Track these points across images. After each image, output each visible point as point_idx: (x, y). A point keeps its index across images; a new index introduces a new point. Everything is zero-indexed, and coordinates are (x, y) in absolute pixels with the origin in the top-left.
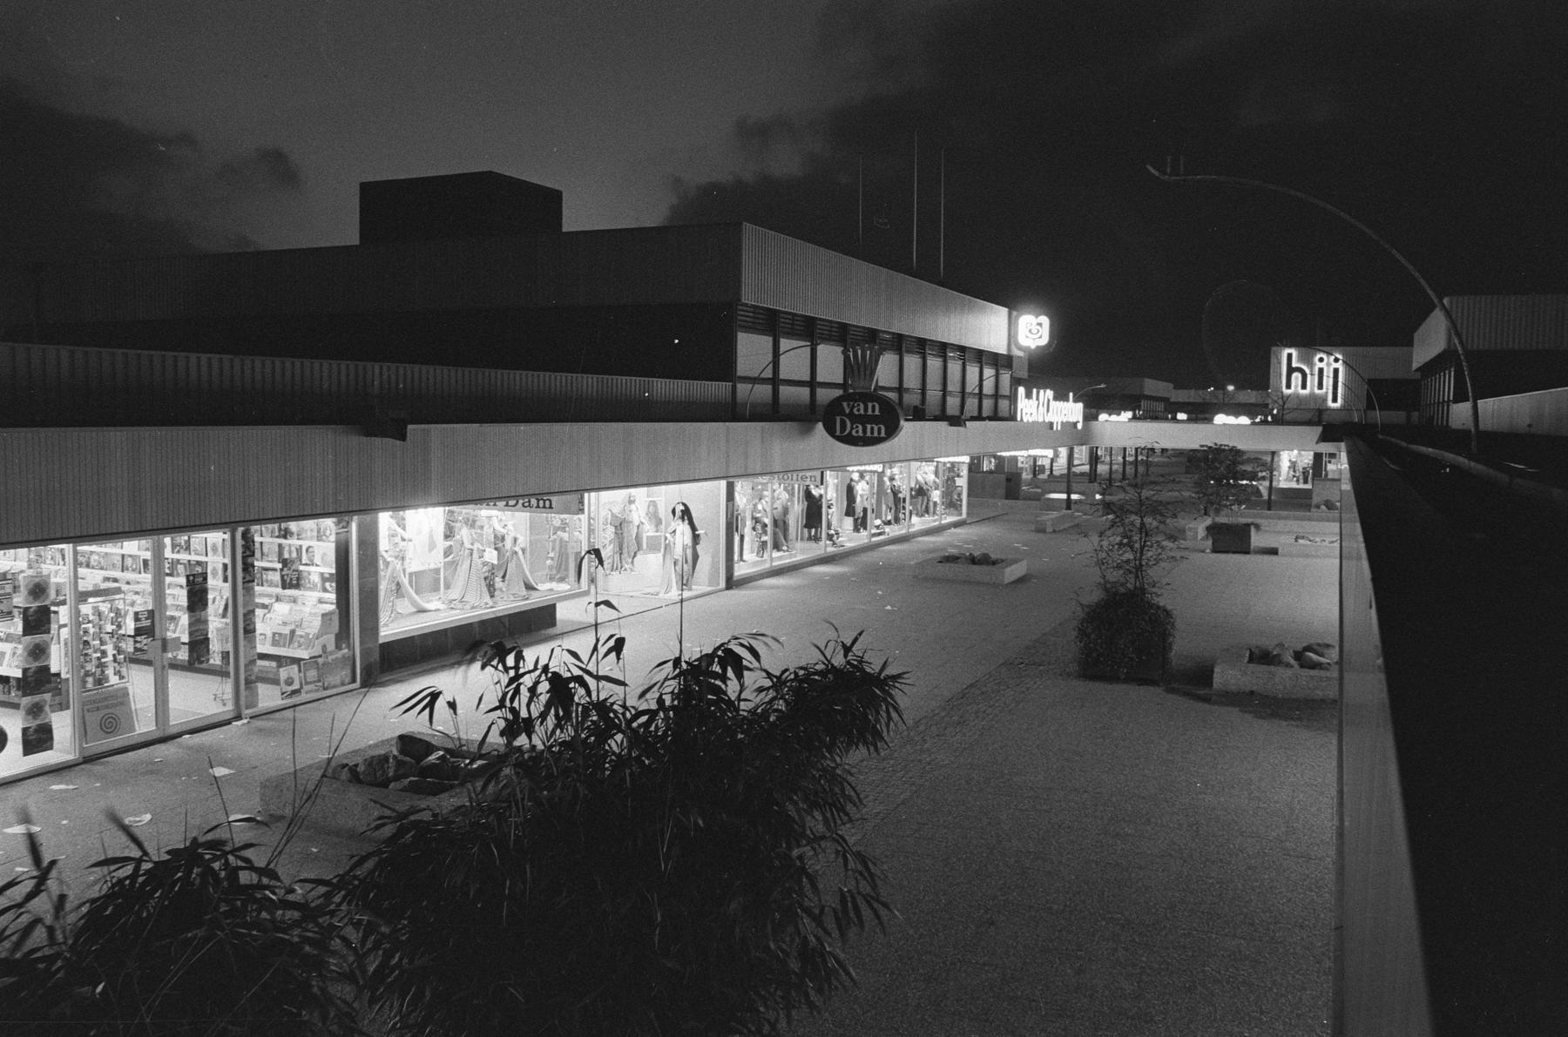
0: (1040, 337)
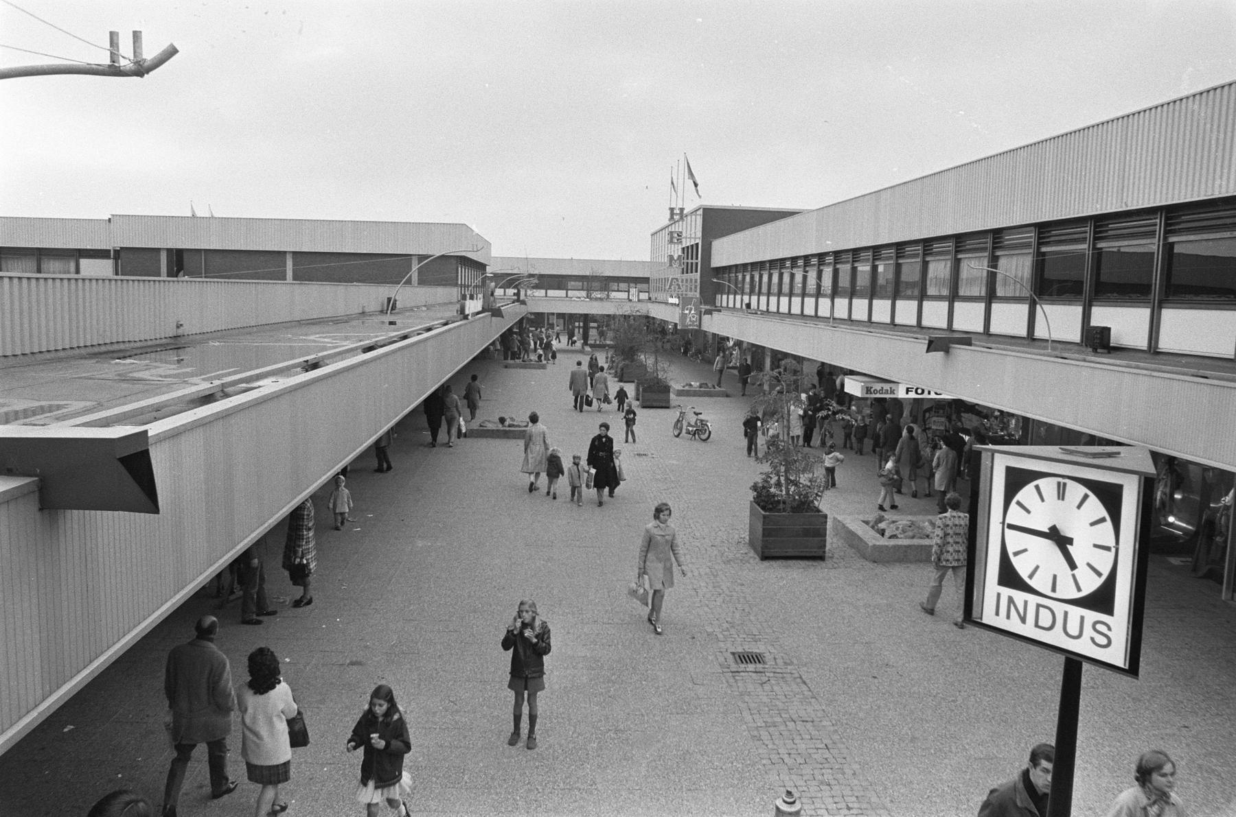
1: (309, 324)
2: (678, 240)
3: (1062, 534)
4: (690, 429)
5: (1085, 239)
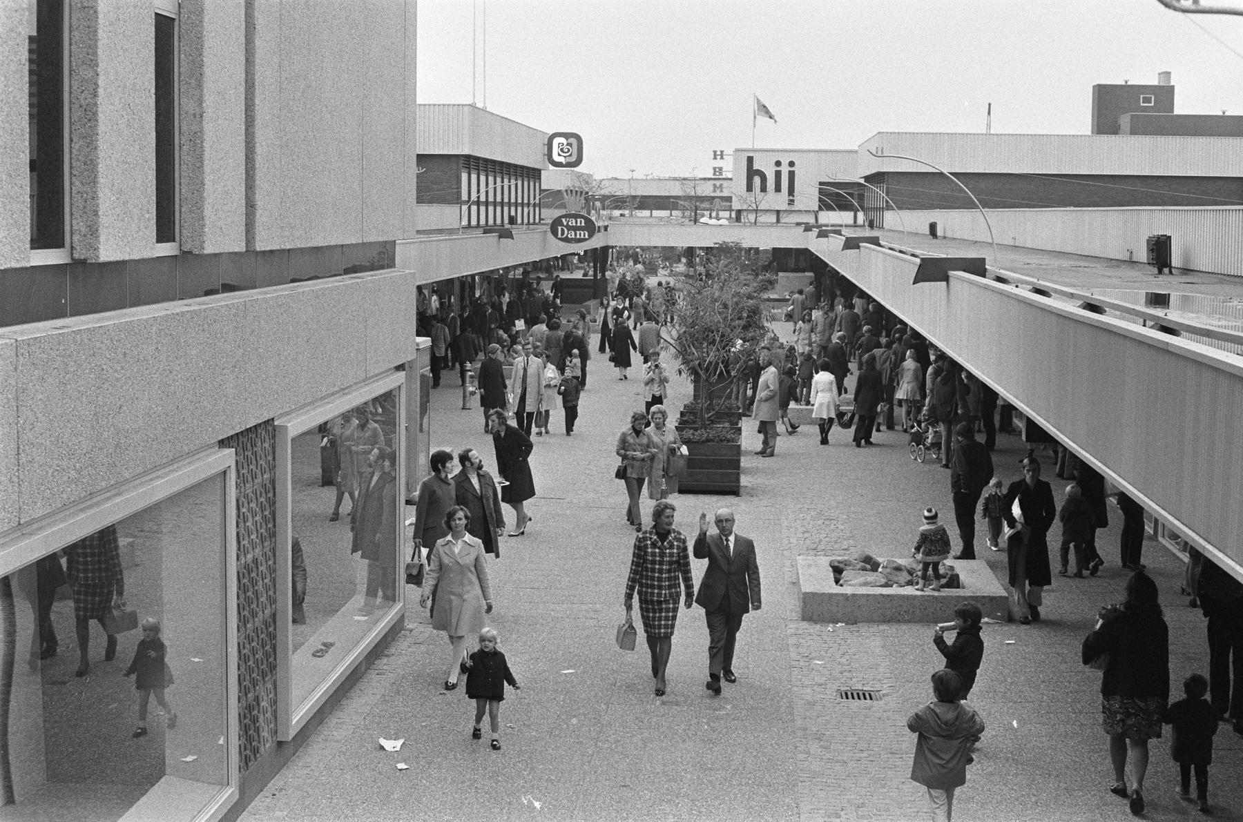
0: (571, 155)
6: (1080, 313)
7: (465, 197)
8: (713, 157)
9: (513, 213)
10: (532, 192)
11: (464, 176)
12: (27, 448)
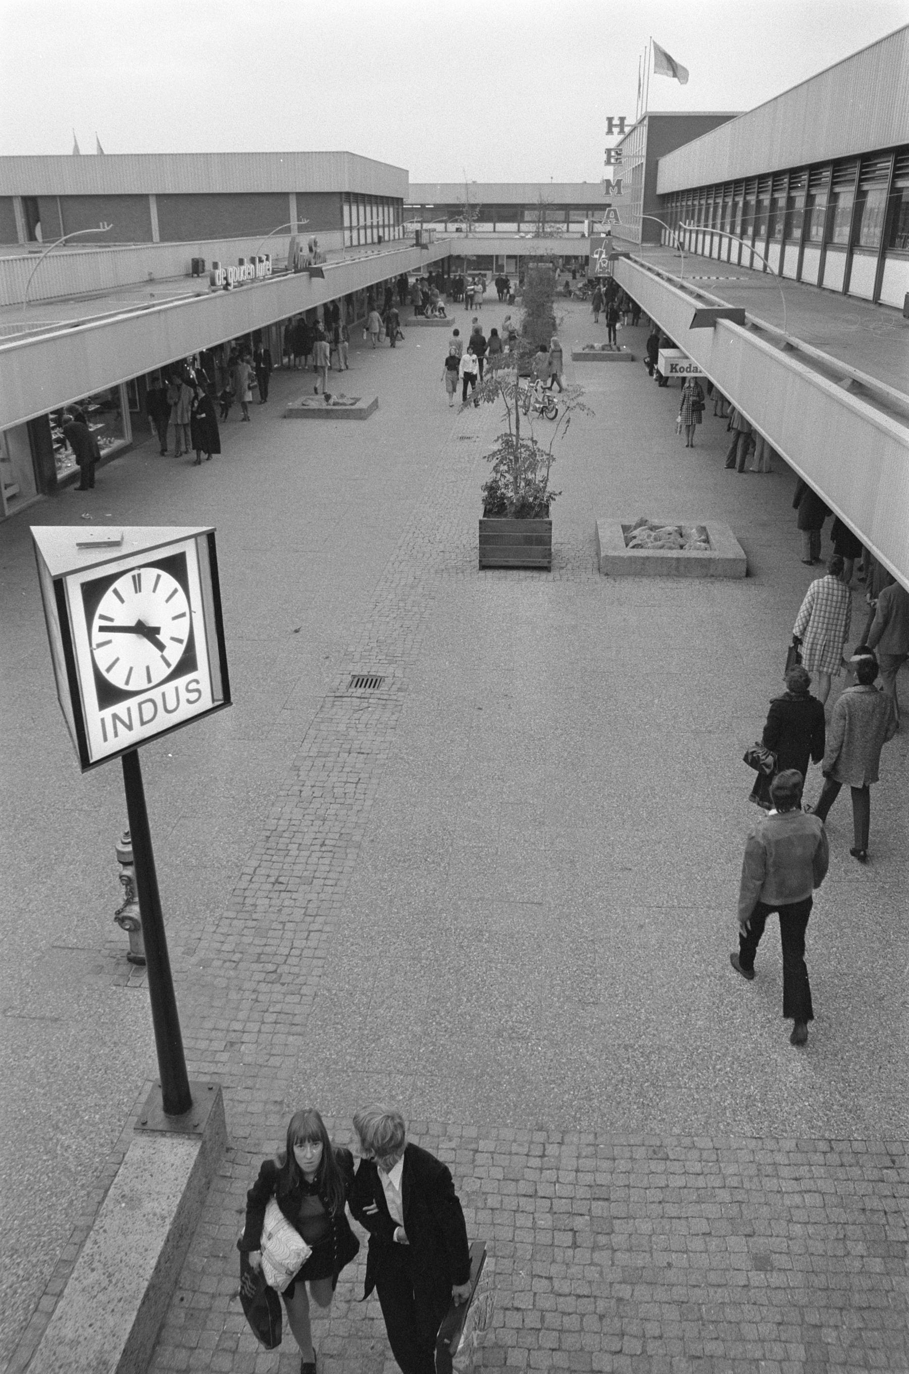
1: (62, 301)
2: (617, 159)
3: (147, 625)
4: (538, 406)
5: (854, 180)
6: (893, 389)
7: (346, 223)
8: (606, 130)
9: (381, 234)
10: (647, 65)
11: (346, 208)
12: (327, 861)
